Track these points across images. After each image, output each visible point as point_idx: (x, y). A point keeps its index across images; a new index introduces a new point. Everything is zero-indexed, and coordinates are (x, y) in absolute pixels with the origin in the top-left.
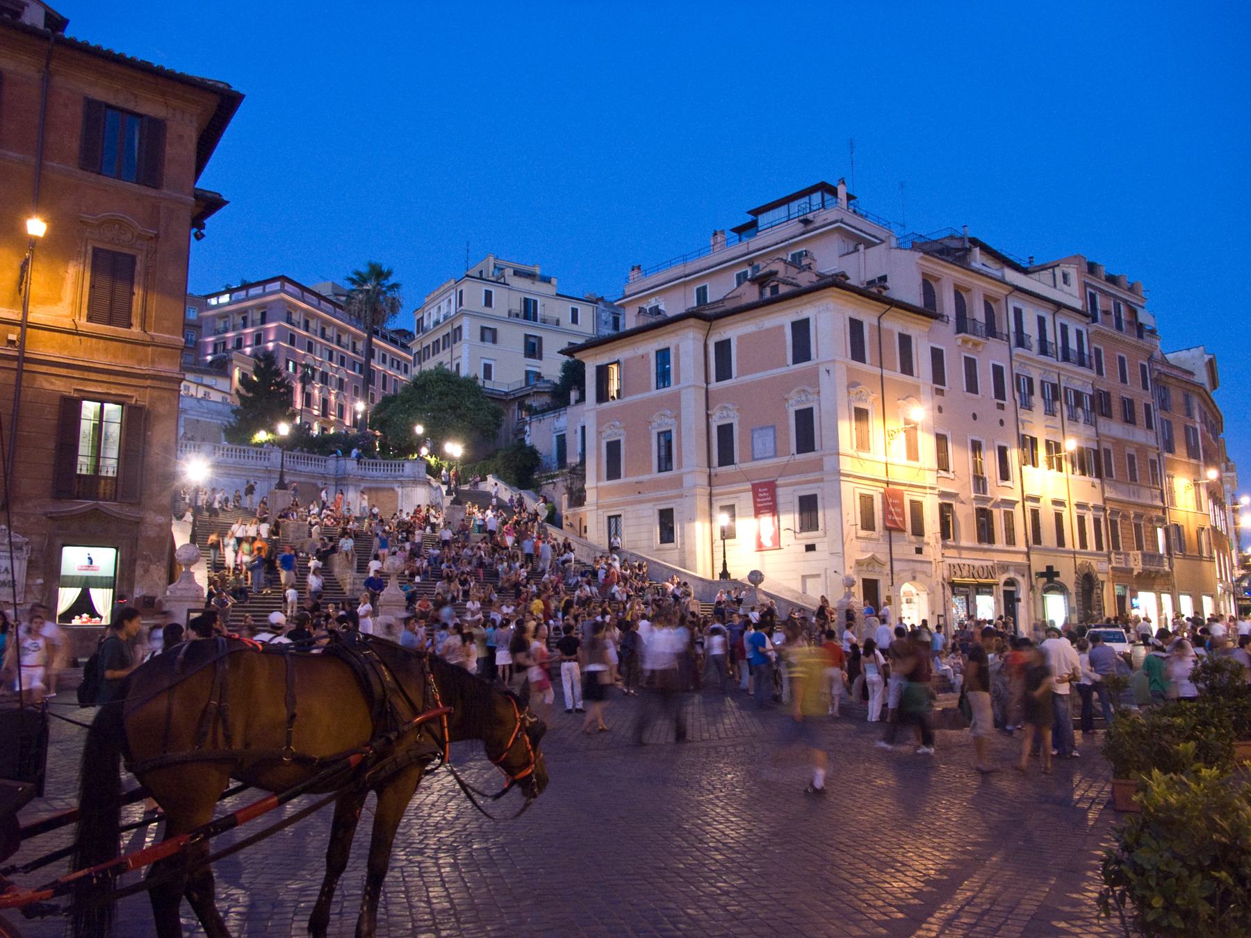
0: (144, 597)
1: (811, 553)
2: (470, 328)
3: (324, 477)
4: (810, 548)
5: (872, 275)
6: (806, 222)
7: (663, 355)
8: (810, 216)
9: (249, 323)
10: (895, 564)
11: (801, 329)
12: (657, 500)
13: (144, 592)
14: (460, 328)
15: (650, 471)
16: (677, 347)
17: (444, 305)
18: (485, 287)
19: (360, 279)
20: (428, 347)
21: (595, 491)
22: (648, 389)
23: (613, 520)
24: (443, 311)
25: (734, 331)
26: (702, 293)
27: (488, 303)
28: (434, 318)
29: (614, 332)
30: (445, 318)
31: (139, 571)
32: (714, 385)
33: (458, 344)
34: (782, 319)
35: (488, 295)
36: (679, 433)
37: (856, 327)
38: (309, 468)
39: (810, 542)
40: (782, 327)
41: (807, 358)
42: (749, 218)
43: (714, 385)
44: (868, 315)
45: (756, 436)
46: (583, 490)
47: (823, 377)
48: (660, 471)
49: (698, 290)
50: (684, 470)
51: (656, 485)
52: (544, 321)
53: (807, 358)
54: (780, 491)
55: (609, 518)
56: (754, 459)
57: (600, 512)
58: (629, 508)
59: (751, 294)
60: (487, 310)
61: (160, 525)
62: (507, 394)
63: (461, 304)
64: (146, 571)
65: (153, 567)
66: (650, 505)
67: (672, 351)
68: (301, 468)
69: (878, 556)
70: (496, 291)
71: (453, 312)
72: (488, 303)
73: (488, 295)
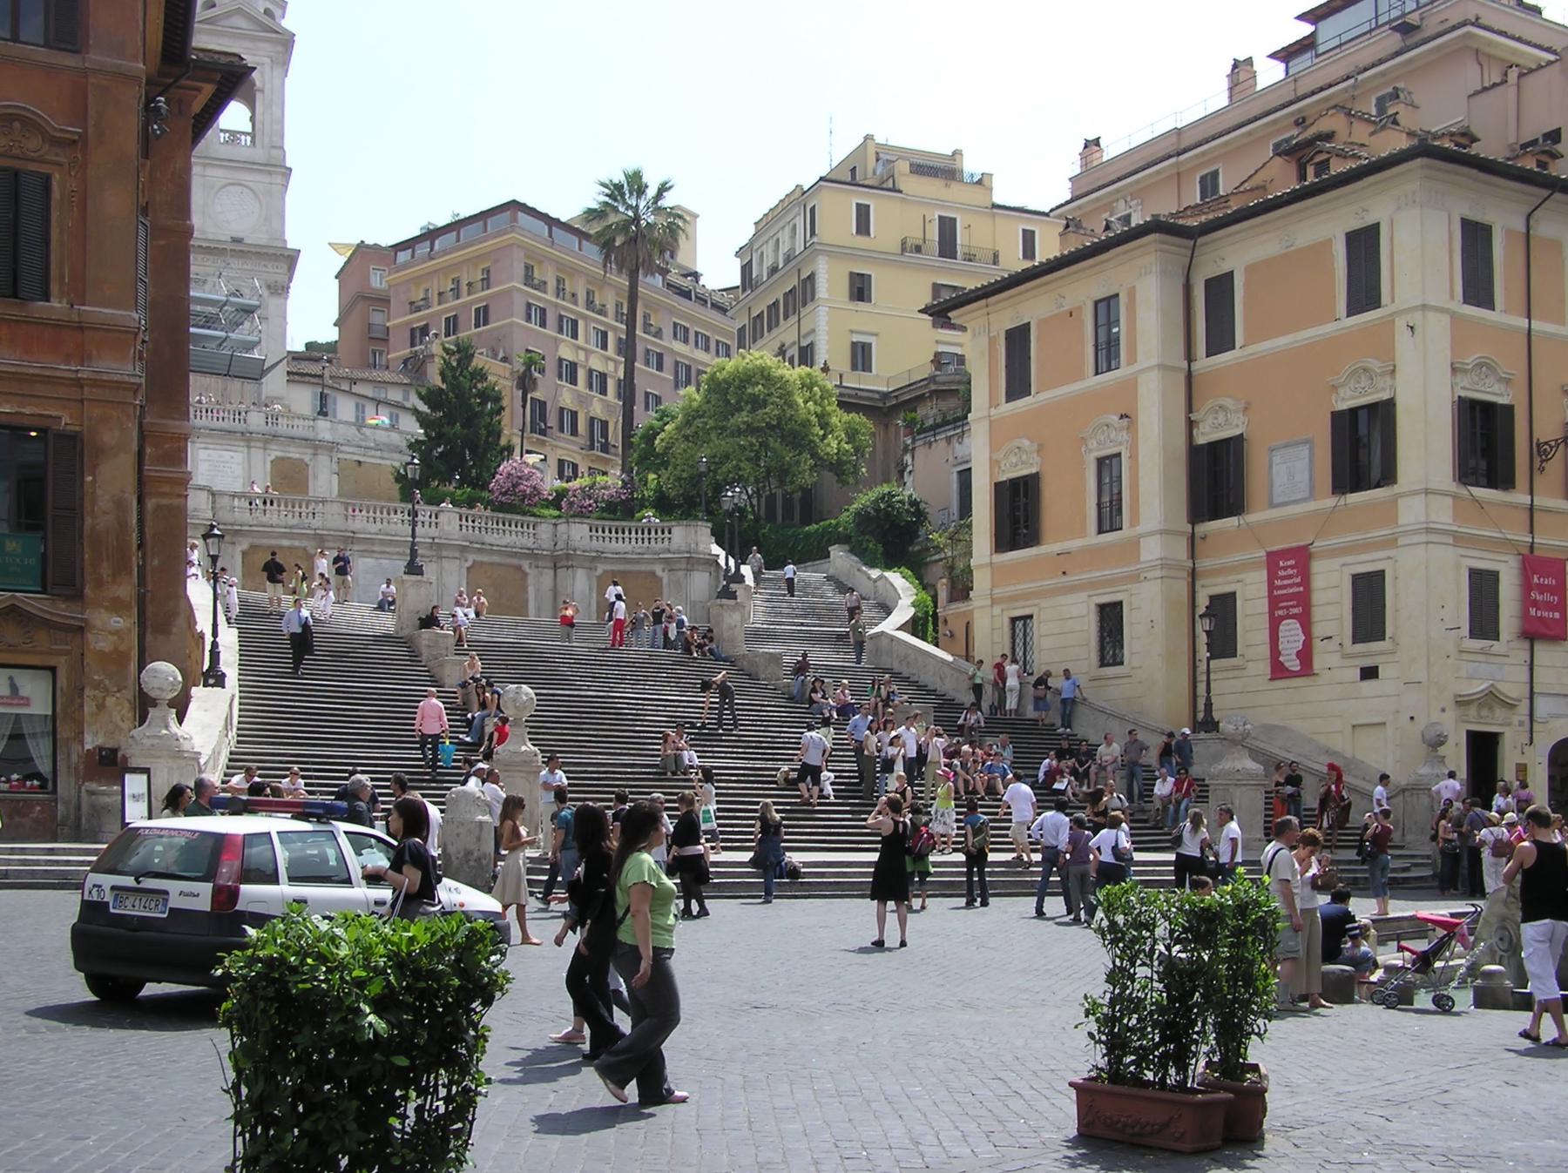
0: (101, 749)
1: (1369, 685)
2: (830, 281)
3: (532, 555)
4: (1369, 673)
5: (1534, 128)
6: (1405, 29)
7: (1106, 308)
8: (1414, 19)
9: (464, 289)
10: (1538, 701)
11: (1364, 246)
12: (1093, 585)
13: (100, 741)
14: (811, 278)
15: (1082, 533)
16: (1132, 293)
17: (784, 236)
18: (857, 198)
19: (616, 191)
20: (760, 316)
21: (988, 571)
22: (1080, 376)
23: (1020, 624)
24: (784, 248)
25: (1237, 254)
26: (1209, 183)
27: (863, 227)
28: (768, 262)
29: (1028, 264)
30: (788, 260)
31: (89, 708)
32: (1203, 363)
33: (810, 307)
34: (1326, 226)
35: (863, 213)
36: (1134, 457)
37: (1476, 238)
38: (508, 539)
39: (1368, 663)
40: (1327, 244)
41: (1375, 303)
42: (1306, 29)
43: (1203, 363)
44: (1503, 216)
45: (1277, 459)
46: (969, 571)
47: (1402, 339)
48: (1100, 531)
49: (1203, 179)
50: (1139, 529)
51: (1093, 555)
52: (970, 258)
53: (1375, 303)
54: (1317, 567)
55: (1014, 620)
56: (1272, 505)
57: (997, 610)
58: (1044, 603)
59: (1283, 179)
60: (862, 241)
61: (117, 632)
62: (885, 396)
63: (813, 233)
64: (101, 707)
65: (110, 701)
66: (1083, 596)
67: (1123, 299)
68: (489, 538)
69: (1501, 686)
70: (880, 208)
71: (799, 247)
72: (863, 227)
73: (863, 213)
